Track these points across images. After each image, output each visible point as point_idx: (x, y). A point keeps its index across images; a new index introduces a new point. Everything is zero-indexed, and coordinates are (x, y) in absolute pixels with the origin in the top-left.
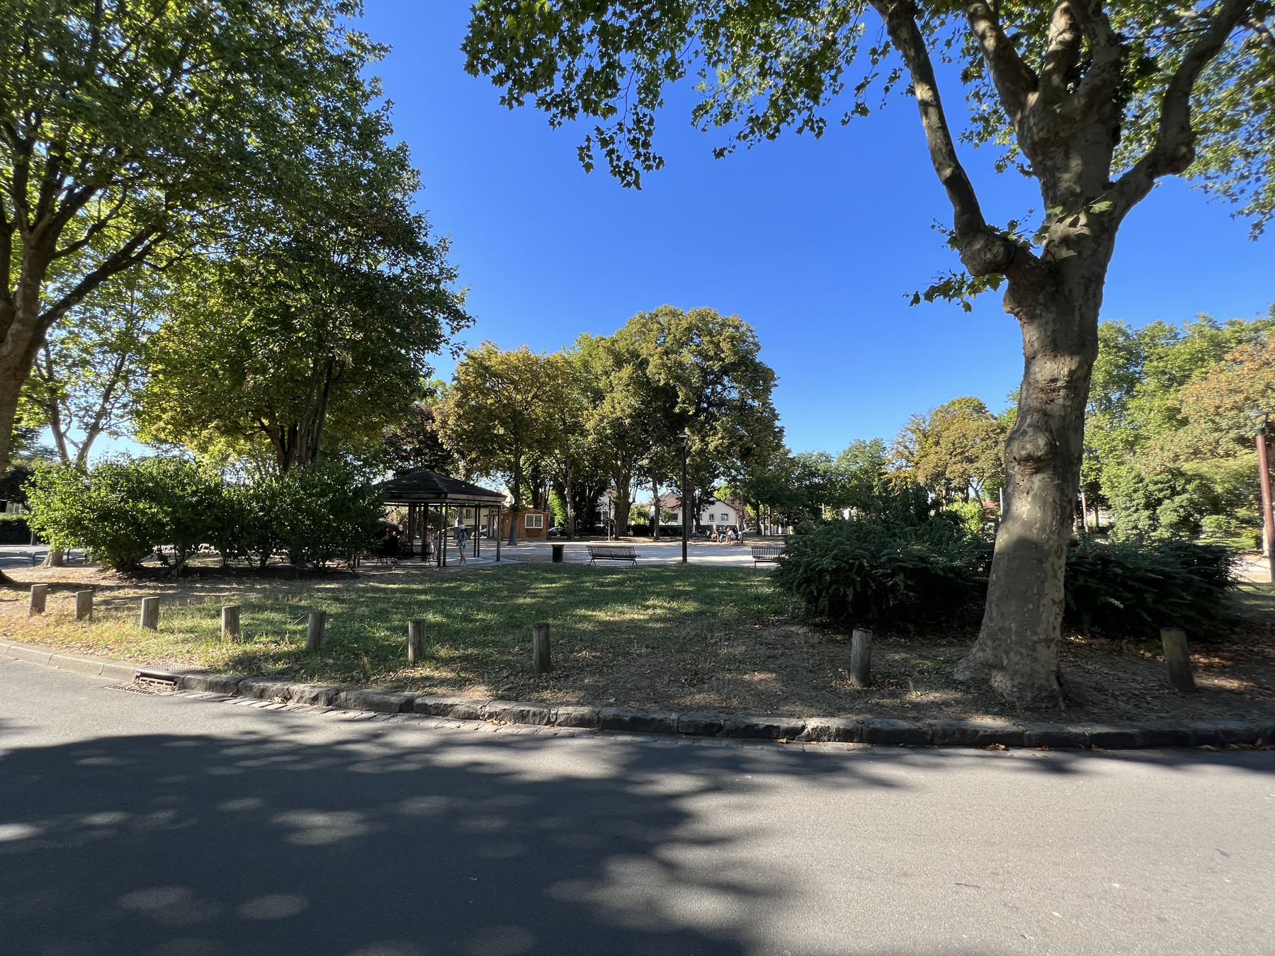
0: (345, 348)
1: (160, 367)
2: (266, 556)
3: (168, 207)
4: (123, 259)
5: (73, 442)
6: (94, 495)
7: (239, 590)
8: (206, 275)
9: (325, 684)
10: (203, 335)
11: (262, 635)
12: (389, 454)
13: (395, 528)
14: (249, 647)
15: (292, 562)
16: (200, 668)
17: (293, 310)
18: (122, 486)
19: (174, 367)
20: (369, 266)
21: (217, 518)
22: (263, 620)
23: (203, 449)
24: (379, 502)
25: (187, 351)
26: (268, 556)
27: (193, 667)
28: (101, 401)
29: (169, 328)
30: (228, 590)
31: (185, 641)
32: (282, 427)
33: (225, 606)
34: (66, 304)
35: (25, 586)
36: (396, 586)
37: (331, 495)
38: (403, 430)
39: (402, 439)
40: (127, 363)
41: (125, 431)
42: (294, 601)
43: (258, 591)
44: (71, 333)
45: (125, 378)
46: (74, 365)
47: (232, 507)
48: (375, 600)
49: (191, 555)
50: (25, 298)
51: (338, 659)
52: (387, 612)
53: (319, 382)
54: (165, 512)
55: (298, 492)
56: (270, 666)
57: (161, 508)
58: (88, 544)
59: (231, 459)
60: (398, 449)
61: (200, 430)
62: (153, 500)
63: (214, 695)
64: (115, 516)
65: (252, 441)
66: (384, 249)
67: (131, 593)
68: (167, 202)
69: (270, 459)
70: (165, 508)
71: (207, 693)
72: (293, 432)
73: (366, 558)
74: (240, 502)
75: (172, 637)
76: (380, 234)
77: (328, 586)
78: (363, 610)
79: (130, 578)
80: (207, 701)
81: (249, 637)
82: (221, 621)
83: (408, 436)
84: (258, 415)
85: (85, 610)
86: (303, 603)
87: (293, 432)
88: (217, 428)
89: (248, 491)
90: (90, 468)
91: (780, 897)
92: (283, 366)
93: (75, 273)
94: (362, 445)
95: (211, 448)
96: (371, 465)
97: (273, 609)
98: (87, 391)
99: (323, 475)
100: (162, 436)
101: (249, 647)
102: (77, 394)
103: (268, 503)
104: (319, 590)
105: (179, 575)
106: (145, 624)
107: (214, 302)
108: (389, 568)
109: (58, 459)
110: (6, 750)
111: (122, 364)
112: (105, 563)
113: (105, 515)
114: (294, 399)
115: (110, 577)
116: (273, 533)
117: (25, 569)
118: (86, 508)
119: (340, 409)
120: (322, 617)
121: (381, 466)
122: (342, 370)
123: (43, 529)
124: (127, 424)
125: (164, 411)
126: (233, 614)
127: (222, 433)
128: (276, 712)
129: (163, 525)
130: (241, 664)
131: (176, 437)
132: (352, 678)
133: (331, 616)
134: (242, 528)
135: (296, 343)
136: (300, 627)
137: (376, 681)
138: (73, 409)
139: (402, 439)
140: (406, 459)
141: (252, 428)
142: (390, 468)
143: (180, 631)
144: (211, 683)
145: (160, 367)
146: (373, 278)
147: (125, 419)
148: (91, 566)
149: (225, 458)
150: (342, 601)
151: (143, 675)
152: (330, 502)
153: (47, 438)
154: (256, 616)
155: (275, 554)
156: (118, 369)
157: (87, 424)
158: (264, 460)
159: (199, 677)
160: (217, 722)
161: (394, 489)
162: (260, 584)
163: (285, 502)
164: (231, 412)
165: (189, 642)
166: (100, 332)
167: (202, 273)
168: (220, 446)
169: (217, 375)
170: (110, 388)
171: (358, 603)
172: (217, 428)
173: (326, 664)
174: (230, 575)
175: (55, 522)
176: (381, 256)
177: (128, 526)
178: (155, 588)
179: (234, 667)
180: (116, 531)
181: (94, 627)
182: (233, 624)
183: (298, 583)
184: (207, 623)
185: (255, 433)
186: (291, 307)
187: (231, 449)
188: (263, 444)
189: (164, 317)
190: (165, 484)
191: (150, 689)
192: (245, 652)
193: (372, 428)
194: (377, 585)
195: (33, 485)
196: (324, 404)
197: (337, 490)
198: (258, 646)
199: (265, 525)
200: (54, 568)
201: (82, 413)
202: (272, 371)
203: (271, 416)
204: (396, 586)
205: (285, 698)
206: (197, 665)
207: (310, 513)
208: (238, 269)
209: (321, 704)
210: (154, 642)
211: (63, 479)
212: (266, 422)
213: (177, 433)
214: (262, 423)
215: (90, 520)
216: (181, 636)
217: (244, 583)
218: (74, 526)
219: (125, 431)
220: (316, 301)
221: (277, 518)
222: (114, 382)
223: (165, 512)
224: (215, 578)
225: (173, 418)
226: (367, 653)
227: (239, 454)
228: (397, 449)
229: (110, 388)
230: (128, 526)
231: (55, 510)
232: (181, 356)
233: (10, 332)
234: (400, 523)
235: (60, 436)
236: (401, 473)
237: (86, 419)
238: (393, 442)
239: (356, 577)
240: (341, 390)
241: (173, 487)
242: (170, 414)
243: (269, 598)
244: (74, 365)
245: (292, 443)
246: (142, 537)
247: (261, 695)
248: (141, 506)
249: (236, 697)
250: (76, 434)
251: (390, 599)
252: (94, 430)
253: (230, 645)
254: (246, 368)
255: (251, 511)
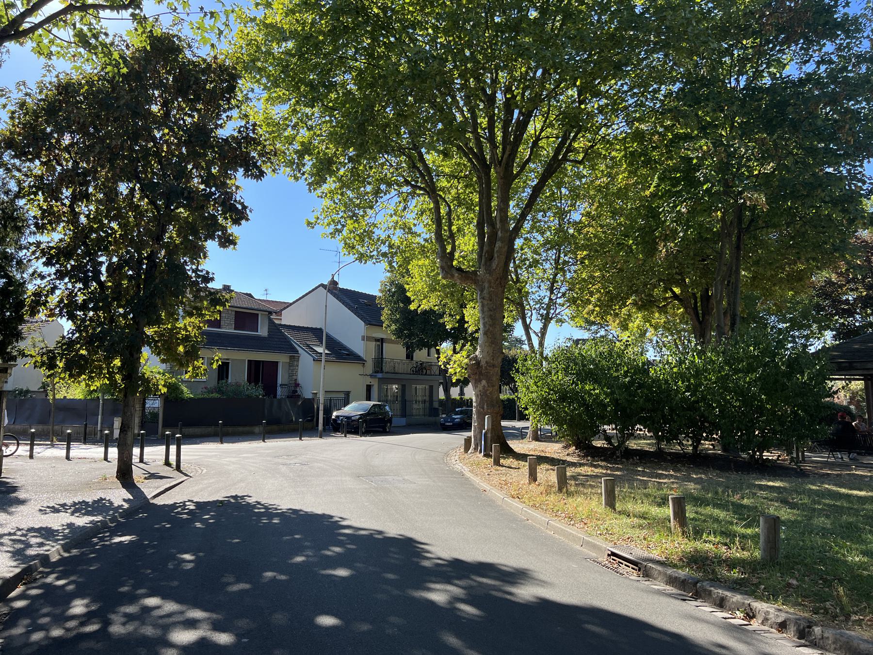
0: (755, 188)
1: (585, 253)
2: (697, 440)
3: (581, 103)
4: (554, 164)
5: (535, 332)
6: (554, 378)
7: (676, 478)
8: (613, 153)
9: (792, 610)
10: (614, 213)
11: (709, 534)
12: (823, 309)
13: (846, 410)
14: (699, 545)
15: (724, 449)
16: (658, 558)
17: (695, 161)
18: (572, 370)
19: (596, 249)
20: (772, 76)
21: (648, 400)
22: (706, 515)
23: (624, 327)
24: (822, 376)
25: (604, 232)
26: (699, 443)
27: (652, 556)
28: (548, 293)
29: (588, 214)
30: (666, 476)
31: (640, 526)
32: (694, 294)
33: (673, 494)
34: (523, 216)
35: (522, 457)
36: (862, 493)
37: (760, 370)
38: (840, 274)
39: (841, 286)
40: (562, 255)
41: (566, 318)
42: (736, 498)
43: (697, 481)
44: (526, 239)
45: (562, 269)
46: (530, 266)
47: (660, 387)
48: (840, 510)
49: (632, 436)
50: (501, 221)
51: (803, 581)
52: (858, 529)
53: (729, 235)
54: (605, 393)
55: (722, 367)
56: (724, 572)
57: (602, 389)
58: (555, 423)
59: (648, 334)
60: (836, 302)
61: (620, 308)
62: (596, 381)
63: (670, 589)
64: (570, 398)
65: (666, 312)
66: (789, 47)
67: (587, 470)
68: (579, 97)
69: (684, 330)
70: (605, 389)
71: (668, 587)
72: (706, 298)
73: (811, 450)
74: (666, 381)
75: (629, 521)
76: (780, 31)
77: (771, 484)
78: (821, 521)
79: (586, 456)
80: (670, 595)
81: (698, 534)
82: (669, 511)
83: (848, 282)
84: (669, 283)
85: (563, 481)
86: (745, 501)
87: (706, 298)
88: (635, 304)
89: (672, 369)
90: (547, 352)
91: (297, 385)
92: (691, 227)
93: (524, 187)
94: (786, 301)
95: (631, 325)
96: (801, 327)
97: (716, 506)
98: (539, 287)
99: (748, 346)
100: (592, 318)
101: (699, 545)
102: (534, 290)
103: (692, 381)
104: (761, 487)
105: (623, 456)
106: (606, 504)
107: (621, 179)
108: (847, 466)
109: (526, 347)
110: (538, 598)
111: (559, 257)
112: (567, 440)
113: (564, 396)
114: (704, 260)
115: (570, 454)
116: (702, 416)
117: (518, 441)
118: (551, 390)
119: (757, 263)
120: (774, 523)
121: (815, 326)
122: (753, 214)
123: (526, 409)
124: (566, 312)
125: (592, 294)
126: (679, 505)
127: (640, 309)
128: (738, 628)
129: (605, 406)
130: (696, 563)
131: (602, 318)
132: (826, 611)
133: (784, 523)
134: (672, 410)
135: (702, 198)
136: (749, 531)
137: (859, 622)
138: (532, 303)
139: (841, 286)
140: (850, 313)
141: (665, 299)
142: (828, 327)
143: (635, 516)
144: (670, 577)
145: (585, 253)
146: (782, 86)
147: (565, 306)
148: (557, 442)
149: (643, 334)
150: (793, 506)
151: (613, 554)
152: (759, 377)
153: (518, 331)
154: (699, 509)
155: (706, 439)
156: (557, 261)
157: (542, 315)
158: (679, 332)
159: (659, 568)
160: (684, 622)
161: (841, 357)
162: (696, 474)
163: (710, 380)
164: (645, 285)
165: (643, 528)
166: (542, 234)
167: (610, 153)
168: (638, 322)
169: (632, 250)
170: (554, 281)
171: (814, 510)
172: (635, 304)
173: (789, 585)
174: (665, 460)
175: (533, 402)
176: (786, 58)
177: (580, 407)
178: (607, 468)
179: (688, 565)
180: (572, 411)
181: (570, 500)
182: (680, 514)
183: (734, 476)
184: (655, 511)
185: (668, 304)
186: (692, 159)
187: (648, 324)
188: (677, 315)
189: (584, 206)
190: (603, 366)
191: (621, 570)
192: (696, 550)
193: (798, 279)
194: (834, 488)
195: (517, 371)
196: (738, 260)
197: (766, 365)
198: (709, 545)
199: (692, 407)
200: (534, 442)
201: (537, 306)
202: (681, 234)
203: (681, 283)
204: (862, 493)
205: (748, 614)
206: (655, 554)
207: (741, 393)
208: (638, 136)
209: (791, 633)
210: (617, 523)
211: (535, 366)
212: (677, 290)
213: (603, 315)
214: (673, 292)
215: (554, 401)
216: (636, 520)
217: (679, 471)
218: (545, 406)
219: (566, 318)
220: (717, 143)
221: (704, 398)
222: (556, 275)
223: (605, 393)
224: (651, 462)
225: (599, 300)
226: (841, 581)
227: (656, 328)
228: (834, 301)
229: (554, 281)
230: (580, 407)
231: (532, 392)
232: (600, 239)
233: (496, 250)
234: (850, 403)
235: (527, 328)
236: (843, 333)
237: (542, 311)
238: (829, 292)
239: (803, 474)
240: (755, 238)
241: (609, 369)
242: (596, 296)
243: (708, 491)
244: (530, 266)
245: (707, 311)
246: (591, 417)
247: (721, 604)
248: (587, 387)
249: (696, 600)
250: (536, 325)
251: (857, 510)
252: (546, 319)
253: (680, 539)
254: (657, 237)
255: (677, 391)
